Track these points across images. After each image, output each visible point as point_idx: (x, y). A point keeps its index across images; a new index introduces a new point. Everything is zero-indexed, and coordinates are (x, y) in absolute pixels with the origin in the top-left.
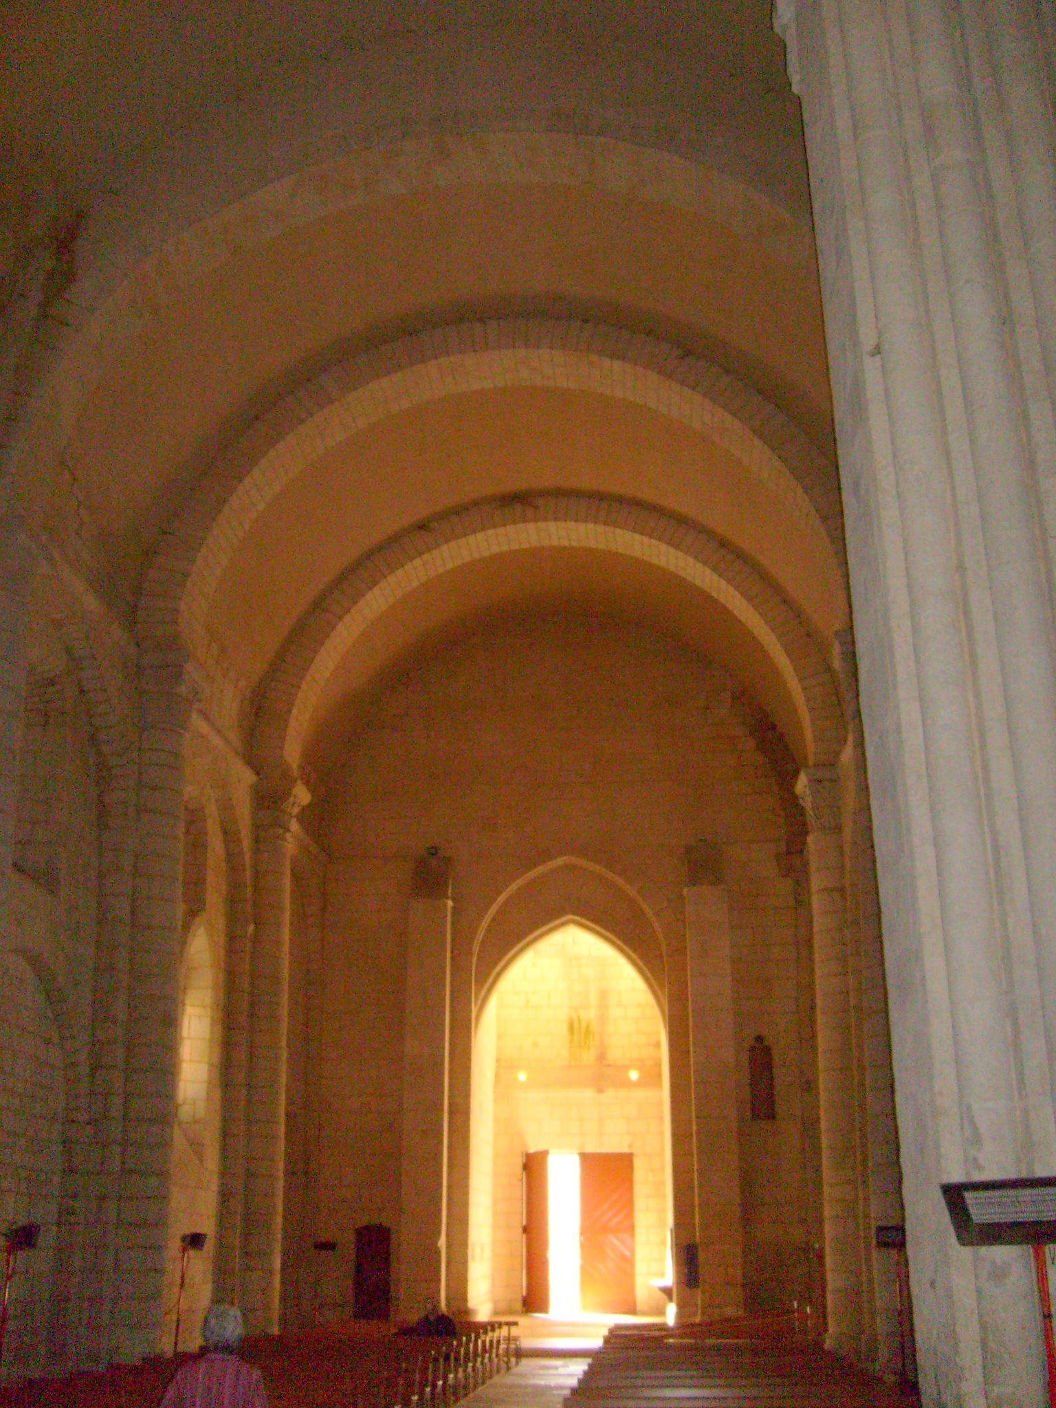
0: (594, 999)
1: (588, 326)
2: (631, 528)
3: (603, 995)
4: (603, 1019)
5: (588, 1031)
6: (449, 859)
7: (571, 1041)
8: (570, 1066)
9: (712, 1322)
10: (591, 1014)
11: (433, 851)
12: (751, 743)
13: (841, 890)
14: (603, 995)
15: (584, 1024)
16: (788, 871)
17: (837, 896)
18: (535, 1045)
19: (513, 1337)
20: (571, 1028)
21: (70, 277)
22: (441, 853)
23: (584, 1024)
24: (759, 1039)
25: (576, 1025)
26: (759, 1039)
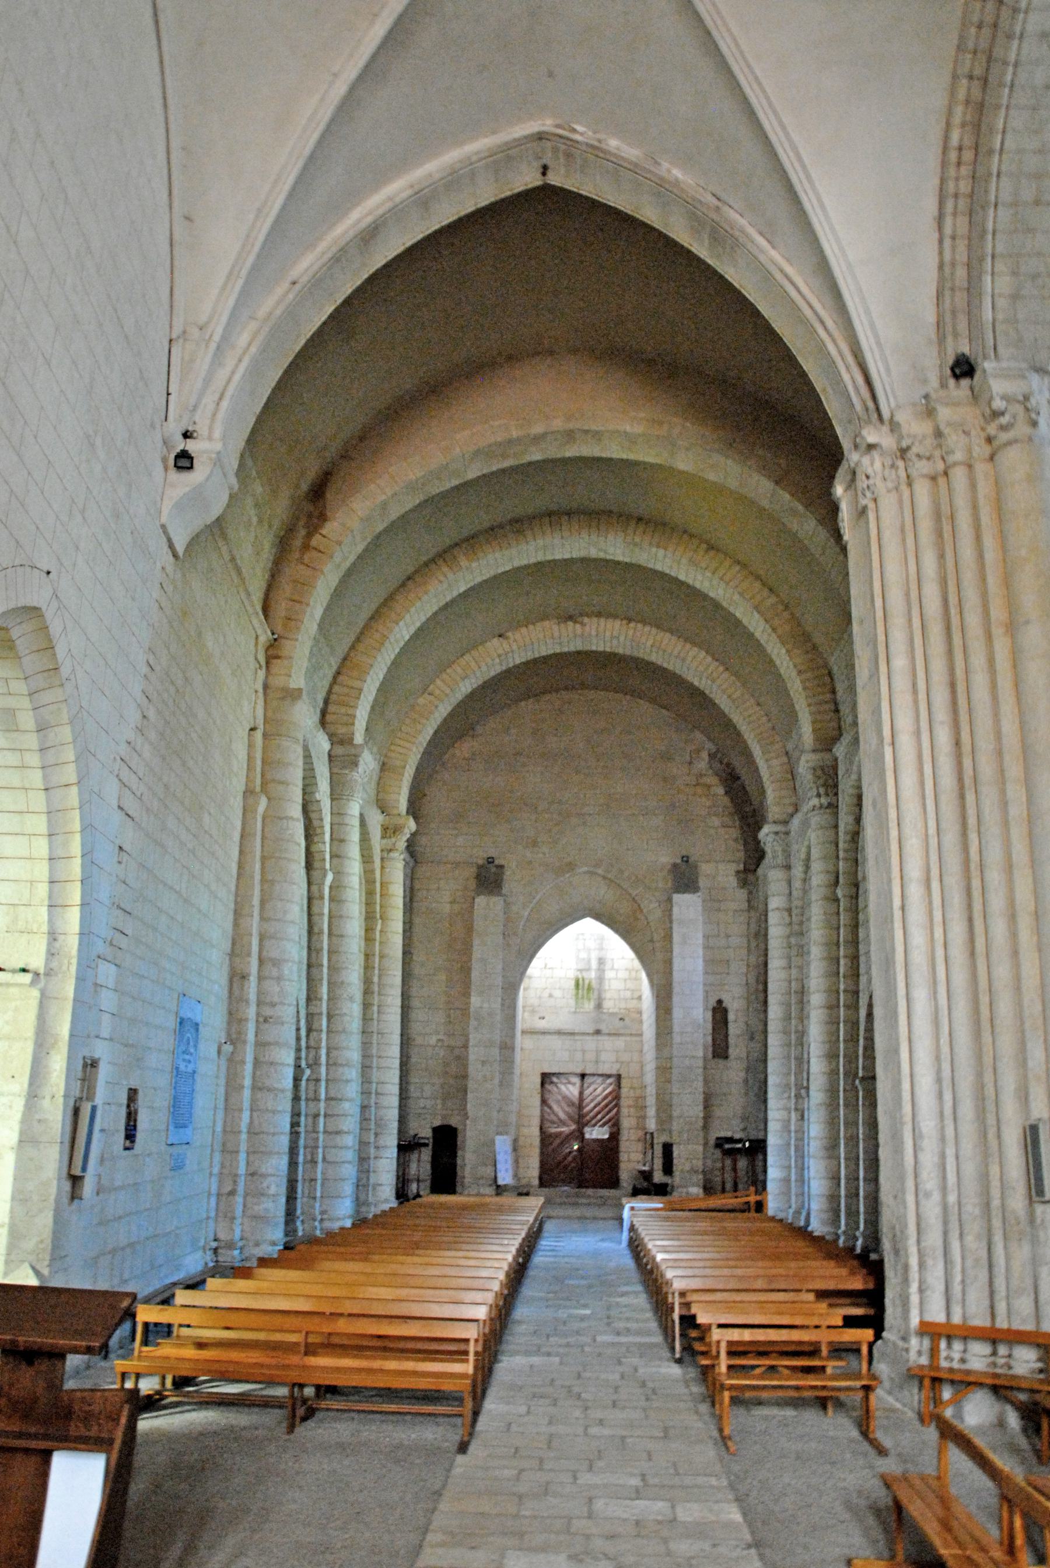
0: (594, 965)
1: (632, 625)
2: (668, 1037)
3: (601, 961)
4: (601, 979)
5: (590, 988)
6: (502, 867)
7: (577, 994)
8: (575, 1012)
9: (637, 523)
10: (593, 975)
11: (490, 860)
12: (721, 791)
13: (789, 910)
14: (601, 961)
15: (587, 982)
16: (744, 883)
17: (786, 914)
18: (551, 996)
19: (533, 1001)
20: (577, 985)
21: (323, 518)
22: (497, 862)
23: (587, 982)
24: (720, 1002)
25: (581, 982)
26: (720, 1002)
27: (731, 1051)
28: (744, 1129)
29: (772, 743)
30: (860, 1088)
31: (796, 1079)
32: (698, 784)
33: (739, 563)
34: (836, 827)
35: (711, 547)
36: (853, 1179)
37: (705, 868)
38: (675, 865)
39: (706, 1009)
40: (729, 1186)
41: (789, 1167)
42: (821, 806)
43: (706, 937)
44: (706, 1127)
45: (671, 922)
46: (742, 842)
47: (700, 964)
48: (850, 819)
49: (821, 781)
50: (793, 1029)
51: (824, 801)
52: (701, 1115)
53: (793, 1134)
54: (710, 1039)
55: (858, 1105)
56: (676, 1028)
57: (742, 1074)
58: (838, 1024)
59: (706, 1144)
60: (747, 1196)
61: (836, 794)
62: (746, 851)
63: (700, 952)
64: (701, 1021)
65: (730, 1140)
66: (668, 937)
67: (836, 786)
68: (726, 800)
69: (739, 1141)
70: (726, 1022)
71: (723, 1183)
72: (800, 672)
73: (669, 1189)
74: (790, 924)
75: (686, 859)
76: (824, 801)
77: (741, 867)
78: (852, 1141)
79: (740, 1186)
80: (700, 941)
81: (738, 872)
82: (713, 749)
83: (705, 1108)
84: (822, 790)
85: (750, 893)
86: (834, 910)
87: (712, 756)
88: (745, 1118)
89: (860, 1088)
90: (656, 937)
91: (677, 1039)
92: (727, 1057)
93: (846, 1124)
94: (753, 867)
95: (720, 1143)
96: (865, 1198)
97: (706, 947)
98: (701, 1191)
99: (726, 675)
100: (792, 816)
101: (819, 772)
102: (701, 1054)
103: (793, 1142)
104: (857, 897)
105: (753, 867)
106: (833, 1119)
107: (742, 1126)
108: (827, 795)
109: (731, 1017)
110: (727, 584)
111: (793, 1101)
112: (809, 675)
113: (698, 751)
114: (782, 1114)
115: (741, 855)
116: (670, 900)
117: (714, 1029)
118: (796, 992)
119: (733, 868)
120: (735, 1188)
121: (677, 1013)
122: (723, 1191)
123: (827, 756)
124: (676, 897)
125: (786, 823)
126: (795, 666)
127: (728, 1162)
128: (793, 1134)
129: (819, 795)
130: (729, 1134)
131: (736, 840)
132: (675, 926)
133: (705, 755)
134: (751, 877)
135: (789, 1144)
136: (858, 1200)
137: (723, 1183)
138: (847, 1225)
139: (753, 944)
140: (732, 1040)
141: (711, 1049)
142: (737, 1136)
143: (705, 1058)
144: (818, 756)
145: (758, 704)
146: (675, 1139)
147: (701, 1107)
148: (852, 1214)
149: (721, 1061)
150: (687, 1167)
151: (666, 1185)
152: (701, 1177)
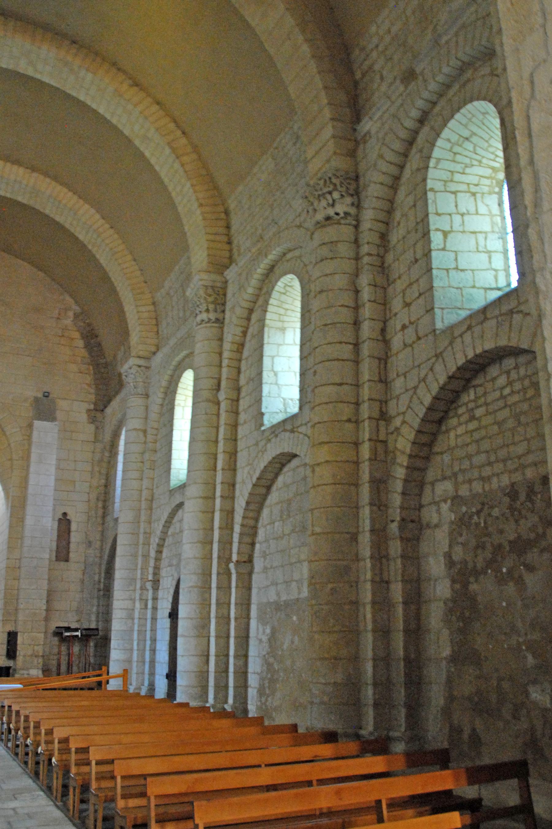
12: (81, 343)
13: (145, 432)
16: (93, 420)
24: (65, 514)
26: (65, 514)
27: (72, 555)
28: (78, 621)
29: (142, 293)
30: (233, 571)
31: (142, 574)
32: (63, 336)
33: (158, 103)
34: (221, 339)
35: (136, 84)
36: (223, 655)
37: (62, 404)
38: (36, 400)
39: (53, 520)
40: (64, 668)
41: (132, 650)
42: (210, 320)
43: (59, 460)
44: (47, 619)
45: (30, 445)
46: (94, 386)
47: (52, 482)
48: (239, 331)
49: (210, 299)
50: (142, 531)
51: (212, 316)
52: (45, 607)
53: (136, 621)
54: (54, 544)
55: (230, 588)
56: (27, 533)
57: (80, 575)
58: (213, 512)
59: (46, 632)
60: (99, 675)
61: (223, 311)
62: (97, 395)
63: (53, 470)
64: (50, 528)
65: (68, 629)
66: (27, 457)
67: (224, 304)
68: (84, 353)
69: (76, 630)
70: (69, 531)
71: (59, 665)
72: (201, 205)
73: (11, 671)
74: (145, 443)
75: (46, 395)
76: (212, 316)
77: (92, 407)
78: (223, 620)
79: (75, 668)
80: (54, 462)
81: (89, 411)
82: (78, 309)
83: (47, 602)
84: (211, 307)
85: (97, 428)
86: (214, 410)
87: (76, 316)
88: (79, 611)
89: (233, 571)
90: (15, 457)
91: (27, 542)
92: (67, 560)
93: (218, 604)
94: (102, 407)
95: (58, 633)
96: (235, 673)
97: (58, 468)
98: (40, 672)
99: (111, 231)
100: (154, 353)
101: (210, 291)
102: (47, 556)
103: (136, 628)
104: (238, 400)
105: (102, 407)
106: (204, 600)
107: (76, 618)
108: (215, 311)
109: (74, 527)
110: (146, 118)
111: (138, 592)
112: (207, 209)
113: (66, 310)
114: (127, 604)
115: (93, 397)
116: (30, 426)
117: (59, 536)
118: (146, 500)
119: (85, 406)
120: (69, 670)
121: (29, 521)
122: (59, 674)
123: (218, 278)
124: (37, 424)
125: (148, 359)
126: (198, 199)
127: (64, 648)
128: (136, 621)
129: (207, 311)
130: (66, 625)
131: (89, 385)
132: (34, 449)
133: (71, 314)
134: (98, 415)
135: (132, 630)
136: (227, 677)
137: (59, 665)
138: (215, 698)
139: (97, 469)
140: (72, 546)
141: (54, 554)
142: (73, 626)
143: (50, 561)
144: (214, 277)
145: (135, 260)
146: (20, 628)
147: (44, 601)
148: (221, 688)
149: (62, 563)
150: (30, 652)
151: (8, 668)
152: (41, 660)
